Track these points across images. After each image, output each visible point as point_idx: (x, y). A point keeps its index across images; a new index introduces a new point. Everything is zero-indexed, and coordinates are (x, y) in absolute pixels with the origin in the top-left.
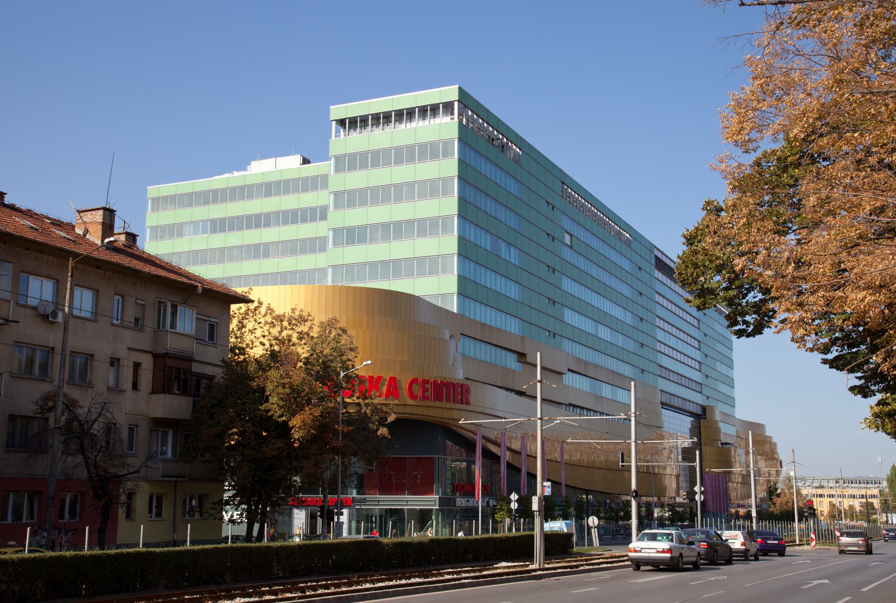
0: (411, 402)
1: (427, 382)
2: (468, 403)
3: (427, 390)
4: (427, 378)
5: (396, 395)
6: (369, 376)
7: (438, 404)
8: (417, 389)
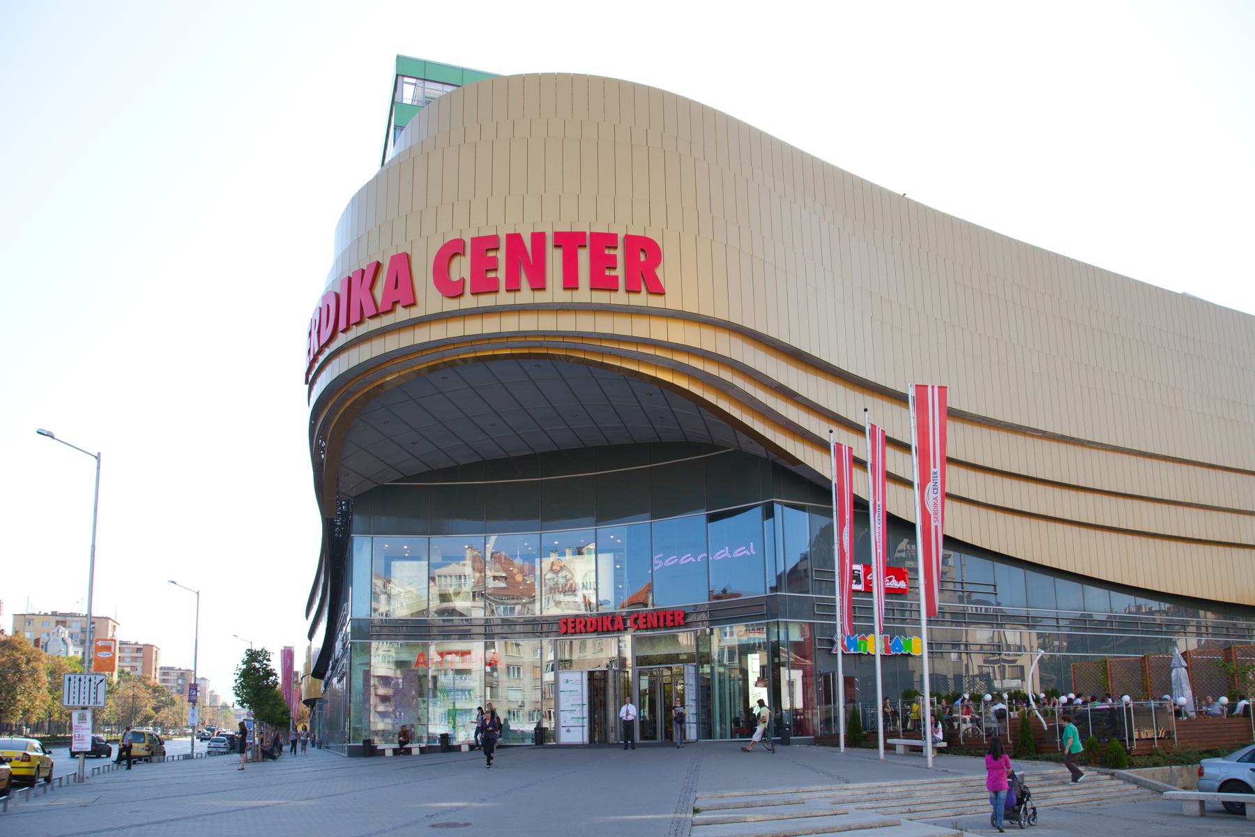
1: (610, 240)
2: (657, 290)
6: (473, 240)
7: (526, 295)
8: (461, 268)
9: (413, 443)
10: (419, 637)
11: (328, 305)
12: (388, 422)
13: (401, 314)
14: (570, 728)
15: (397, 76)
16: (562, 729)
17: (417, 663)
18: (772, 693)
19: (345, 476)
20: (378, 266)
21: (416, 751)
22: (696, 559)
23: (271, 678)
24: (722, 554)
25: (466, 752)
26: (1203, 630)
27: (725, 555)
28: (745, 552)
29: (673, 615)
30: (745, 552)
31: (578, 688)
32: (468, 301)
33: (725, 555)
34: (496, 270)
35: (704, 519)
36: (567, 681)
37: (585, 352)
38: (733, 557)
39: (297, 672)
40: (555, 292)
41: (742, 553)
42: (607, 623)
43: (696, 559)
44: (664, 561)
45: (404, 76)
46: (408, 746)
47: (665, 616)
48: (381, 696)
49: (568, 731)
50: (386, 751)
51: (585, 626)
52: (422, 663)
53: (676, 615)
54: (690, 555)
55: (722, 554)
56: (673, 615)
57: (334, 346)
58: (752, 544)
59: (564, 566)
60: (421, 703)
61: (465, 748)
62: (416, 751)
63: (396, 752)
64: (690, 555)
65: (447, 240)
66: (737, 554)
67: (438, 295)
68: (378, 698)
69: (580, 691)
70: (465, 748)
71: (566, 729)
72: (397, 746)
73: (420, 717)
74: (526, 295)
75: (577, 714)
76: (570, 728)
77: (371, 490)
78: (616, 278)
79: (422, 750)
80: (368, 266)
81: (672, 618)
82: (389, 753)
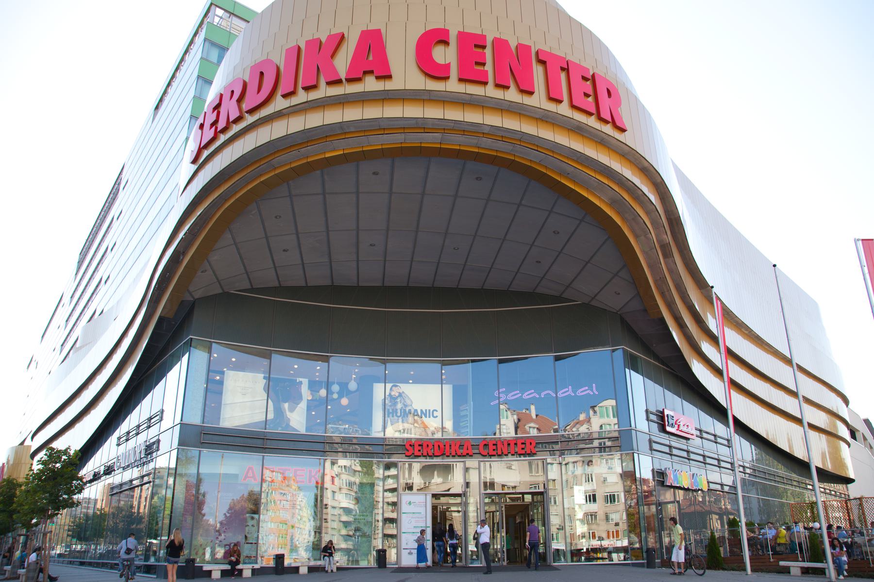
7: (512, 95)
9: (284, 250)
10: (216, 445)
11: (262, 74)
12: (280, 217)
13: (371, 84)
15: (212, 4)
16: (403, 551)
17: (246, 477)
19: (202, 272)
21: (247, 573)
22: (540, 395)
23: (74, 482)
24: (565, 392)
25: (304, 575)
27: (567, 393)
28: (534, 395)
30: (534, 395)
31: (422, 510)
32: (453, 85)
33: (567, 393)
35: (552, 359)
36: (410, 503)
38: (576, 395)
39: (440, 499)
40: (538, 100)
41: (585, 393)
43: (540, 395)
44: (507, 396)
45: (217, 6)
46: (239, 567)
48: (344, 522)
50: (213, 572)
52: (250, 477)
54: (587, 388)
55: (565, 392)
57: (218, 144)
58: (594, 385)
59: (403, 392)
60: (249, 519)
61: (303, 570)
62: (247, 573)
63: (224, 573)
64: (519, 392)
66: (579, 393)
68: (341, 524)
69: (423, 513)
70: (303, 570)
72: (228, 567)
73: (247, 535)
74: (512, 95)
77: (216, 294)
79: (254, 571)
80: (330, 37)
81: (494, 447)
82: (216, 575)
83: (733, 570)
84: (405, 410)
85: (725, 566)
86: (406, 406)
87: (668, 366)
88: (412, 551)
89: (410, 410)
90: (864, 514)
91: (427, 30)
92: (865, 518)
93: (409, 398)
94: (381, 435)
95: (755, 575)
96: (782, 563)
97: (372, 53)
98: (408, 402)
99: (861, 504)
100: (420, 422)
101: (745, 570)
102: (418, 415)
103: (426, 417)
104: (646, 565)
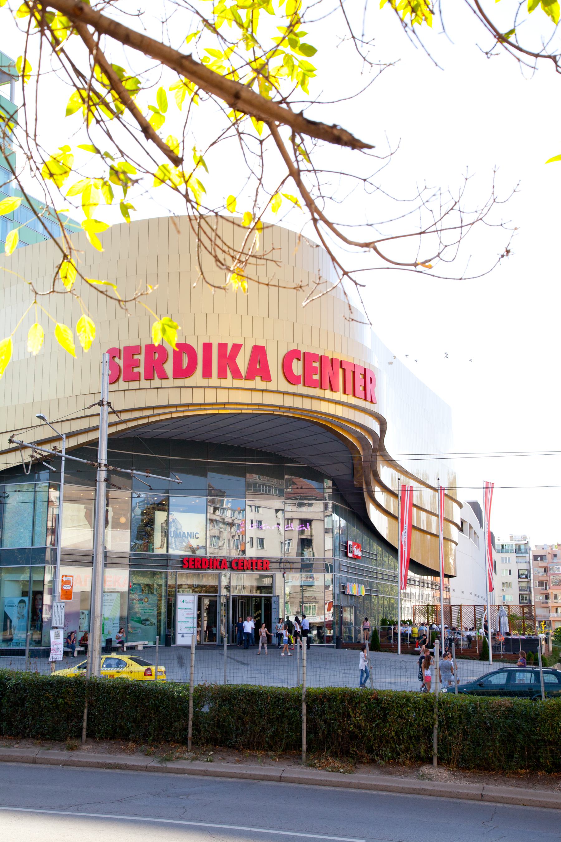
0: (284, 386)
1: (136, 350)
3: (137, 364)
4: (134, 343)
5: (267, 377)
8: (297, 368)
14: (184, 635)
18: (30, 611)
20: (237, 347)
26: (426, 585)
29: (243, 562)
31: (191, 606)
34: (140, 354)
36: (183, 601)
37: (318, 419)
42: (191, 563)
47: (257, 563)
49: (183, 636)
51: (201, 564)
53: (196, 562)
56: (194, 561)
65: (291, 348)
67: (286, 382)
69: (192, 608)
71: (181, 635)
75: (190, 625)
76: (184, 635)
78: (139, 373)
83: (386, 651)
84: (177, 532)
85: (381, 649)
86: (177, 529)
87: (350, 507)
88: (84, 611)
89: (180, 533)
90: (461, 616)
91: (184, 380)
92: (461, 619)
93: (180, 524)
94: (163, 551)
95: (403, 655)
96: (416, 649)
97: (158, 375)
98: (179, 527)
99: (460, 610)
100: (198, 221)
101: (397, 652)
102: (185, 537)
103: (191, 538)
104: (335, 647)
